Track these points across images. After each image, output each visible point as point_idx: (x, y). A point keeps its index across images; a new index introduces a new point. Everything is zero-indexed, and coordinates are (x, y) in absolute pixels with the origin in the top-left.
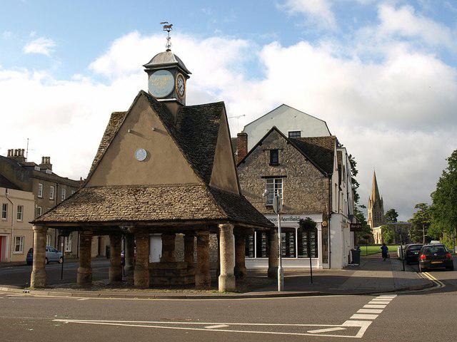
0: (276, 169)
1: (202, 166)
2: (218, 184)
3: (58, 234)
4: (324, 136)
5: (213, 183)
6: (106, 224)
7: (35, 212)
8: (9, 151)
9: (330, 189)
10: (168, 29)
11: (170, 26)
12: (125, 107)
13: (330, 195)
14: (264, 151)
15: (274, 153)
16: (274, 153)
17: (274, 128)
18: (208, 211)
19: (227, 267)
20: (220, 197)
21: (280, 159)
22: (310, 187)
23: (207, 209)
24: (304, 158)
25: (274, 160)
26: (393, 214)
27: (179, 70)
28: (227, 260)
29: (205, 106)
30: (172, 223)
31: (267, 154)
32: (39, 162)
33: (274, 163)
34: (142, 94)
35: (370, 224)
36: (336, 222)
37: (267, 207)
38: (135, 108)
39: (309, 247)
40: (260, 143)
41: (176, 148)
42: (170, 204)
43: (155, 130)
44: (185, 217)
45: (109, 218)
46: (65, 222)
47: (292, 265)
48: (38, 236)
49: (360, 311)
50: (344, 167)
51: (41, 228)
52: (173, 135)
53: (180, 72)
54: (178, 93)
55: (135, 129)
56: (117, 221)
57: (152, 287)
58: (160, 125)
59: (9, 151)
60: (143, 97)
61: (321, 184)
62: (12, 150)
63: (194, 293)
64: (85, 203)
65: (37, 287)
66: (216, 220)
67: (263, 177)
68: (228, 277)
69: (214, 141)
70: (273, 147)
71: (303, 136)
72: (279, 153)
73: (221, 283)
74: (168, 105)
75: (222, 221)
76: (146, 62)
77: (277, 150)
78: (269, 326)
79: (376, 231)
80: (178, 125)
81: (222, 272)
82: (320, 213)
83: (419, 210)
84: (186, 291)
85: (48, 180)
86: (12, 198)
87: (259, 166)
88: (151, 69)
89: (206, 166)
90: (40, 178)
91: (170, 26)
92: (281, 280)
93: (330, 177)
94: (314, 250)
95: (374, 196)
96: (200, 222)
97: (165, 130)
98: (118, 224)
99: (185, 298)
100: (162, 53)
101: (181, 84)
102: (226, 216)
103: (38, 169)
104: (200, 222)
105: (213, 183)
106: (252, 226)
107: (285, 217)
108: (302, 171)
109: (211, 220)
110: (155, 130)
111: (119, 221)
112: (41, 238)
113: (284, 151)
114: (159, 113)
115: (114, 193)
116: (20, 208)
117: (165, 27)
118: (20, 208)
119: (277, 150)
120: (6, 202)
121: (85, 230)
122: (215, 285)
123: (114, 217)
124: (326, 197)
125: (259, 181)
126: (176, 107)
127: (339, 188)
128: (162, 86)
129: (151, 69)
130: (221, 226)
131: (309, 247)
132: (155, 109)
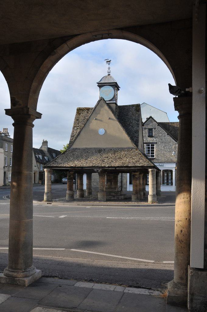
0: (152, 139)
1: (134, 137)
6: (86, 168)
7: (4, 160)
10: (109, 63)
11: (109, 61)
14: (145, 129)
15: (150, 130)
16: (150, 130)
21: (153, 134)
22: (169, 149)
25: (151, 134)
29: (130, 106)
30: (123, 168)
31: (147, 131)
33: (151, 136)
39: (168, 181)
42: (120, 158)
43: (109, 119)
45: (88, 165)
48: (48, 174)
51: (49, 170)
54: (115, 98)
56: (93, 167)
60: (102, 101)
66: (147, 167)
68: (153, 196)
70: (150, 127)
73: (150, 199)
75: (151, 167)
76: (98, 81)
77: (152, 129)
82: (175, 162)
90: (6, 141)
91: (109, 61)
94: (170, 181)
108: (165, 140)
109: (145, 167)
110: (109, 119)
111: (94, 167)
113: (156, 129)
115: (88, 152)
117: (107, 62)
119: (152, 129)
121: (71, 171)
122: (146, 200)
123: (91, 165)
126: (114, 105)
128: (108, 93)
130: (150, 170)
131: (168, 181)
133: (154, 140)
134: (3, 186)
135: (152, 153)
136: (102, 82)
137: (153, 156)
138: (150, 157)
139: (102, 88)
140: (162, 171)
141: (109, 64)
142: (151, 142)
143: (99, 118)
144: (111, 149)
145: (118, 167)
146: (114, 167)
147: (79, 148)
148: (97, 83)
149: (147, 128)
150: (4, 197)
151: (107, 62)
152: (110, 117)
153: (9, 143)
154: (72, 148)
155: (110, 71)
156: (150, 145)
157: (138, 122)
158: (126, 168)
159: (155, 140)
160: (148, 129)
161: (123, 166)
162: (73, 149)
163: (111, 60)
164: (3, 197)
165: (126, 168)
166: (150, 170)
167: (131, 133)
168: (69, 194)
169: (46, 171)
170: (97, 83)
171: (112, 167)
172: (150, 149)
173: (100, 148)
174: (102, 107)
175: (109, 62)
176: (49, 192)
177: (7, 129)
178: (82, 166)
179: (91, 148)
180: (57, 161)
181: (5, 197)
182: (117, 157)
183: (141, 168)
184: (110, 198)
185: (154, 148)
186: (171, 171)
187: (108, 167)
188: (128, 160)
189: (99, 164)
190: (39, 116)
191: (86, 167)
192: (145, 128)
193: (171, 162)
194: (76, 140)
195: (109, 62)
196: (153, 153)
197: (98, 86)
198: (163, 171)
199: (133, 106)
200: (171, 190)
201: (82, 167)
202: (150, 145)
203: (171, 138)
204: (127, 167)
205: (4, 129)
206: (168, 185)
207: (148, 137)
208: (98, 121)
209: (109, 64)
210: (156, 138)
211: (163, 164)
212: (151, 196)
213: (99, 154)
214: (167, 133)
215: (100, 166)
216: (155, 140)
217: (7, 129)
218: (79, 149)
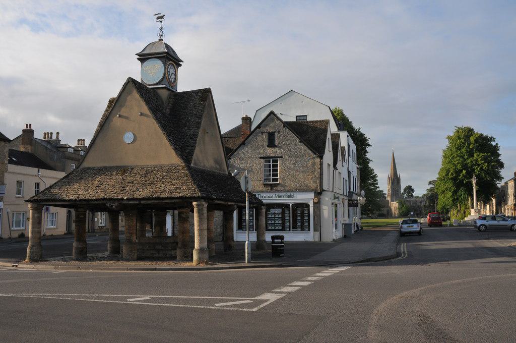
1: (184, 147)
4: (319, 119)
5: (195, 164)
6: (94, 202)
9: (321, 168)
10: (161, 20)
11: (162, 17)
13: (321, 174)
14: (262, 133)
15: (271, 136)
16: (271, 136)
17: (272, 113)
18: (188, 189)
19: (201, 242)
20: (200, 176)
22: (303, 166)
23: (184, 187)
24: (298, 141)
26: (410, 189)
27: (170, 59)
28: (200, 235)
29: (193, 92)
30: (152, 202)
31: (265, 136)
33: (271, 144)
35: (389, 199)
36: (327, 199)
37: (265, 185)
39: (303, 223)
41: (160, 131)
43: (142, 114)
44: (163, 195)
45: (97, 197)
47: (291, 237)
48: (33, 214)
49: (320, 278)
50: (343, 149)
52: (157, 119)
53: (172, 60)
54: (169, 81)
55: (121, 113)
56: (103, 199)
57: (140, 259)
58: (145, 109)
61: (314, 164)
62: (48, 133)
63: (172, 264)
64: (77, 182)
65: (33, 260)
67: (261, 158)
70: (270, 129)
71: (309, 119)
72: (276, 136)
74: (160, 91)
76: (139, 51)
78: (168, 298)
79: (394, 205)
80: (168, 110)
81: (197, 245)
83: (432, 186)
84: (165, 263)
86: (42, 177)
87: (258, 147)
88: (143, 58)
89: (189, 148)
90: (72, 159)
91: (162, 17)
92: (248, 253)
93: (321, 157)
95: (393, 172)
96: (177, 201)
97: (150, 114)
98: (105, 202)
99: (155, 269)
100: (154, 43)
101: (172, 71)
102: (199, 194)
103: (71, 150)
104: (177, 201)
107: (280, 194)
109: (186, 198)
110: (142, 114)
112: (36, 215)
113: (281, 133)
114: (148, 102)
117: (158, 18)
120: (37, 180)
122: (191, 259)
123: (102, 196)
124: (318, 176)
128: (153, 73)
129: (143, 58)
131: (303, 223)
132: (141, 95)
133: (277, 151)
134: (65, 234)
135: (274, 175)
136: (145, 52)
137: (277, 180)
138: (271, 182)
139: (146, 63)
140: (291, 205)
141: (161, 22)
142: (271, 155)
143: (124, 115)
145: (143, 199)
146: (137, 199)
147: (93, 168)
151: (158, 18)
152: (142, 112)
154: (82, 167)
156: (271, 161)
157: (199, 119)
158: (157, 202)
159: (278, 151)
161: (151, 197)
162: (84, 168)
163: (164, 15)
165: (157, 202)
166: (194, 203)
167: (184, 139)
168: (77, 248)
169: (31, 207)
171: (133, 199)
172: (271, 168)
174: (130, 93)
175: (161, 18)
176: (34, 244)
177: (84, 140)
178: (87, 198)
182: (148, 182)
183: (181, 200)
184: (152, 254)
185: (277, 166)
186: (308, 206)
187: (128, 199)
188: (163, 186)
189: (116, 195)
190: (449, 137)
191: (93, 200)
193: (306, 190)
194: (89, 154)
195: (161, 18)
196: (277, 175)
197: (138, 59)
198: (293, 205)
199: (198, 91)
200: (307, 240)
201: (88, 201)
202: (271, 161)
203: (306, 148)
204: (158, 198)
205: (79, 140)
206: (303, 229)
207: (268, 146)
208: (124, 120)
209: (161, 22)
210: (280, 148)
211: (292, 194)
212: (196, 251)
214: (299, 138)
215: (115, 197)
216: (278, 151)
217: (84, 140)
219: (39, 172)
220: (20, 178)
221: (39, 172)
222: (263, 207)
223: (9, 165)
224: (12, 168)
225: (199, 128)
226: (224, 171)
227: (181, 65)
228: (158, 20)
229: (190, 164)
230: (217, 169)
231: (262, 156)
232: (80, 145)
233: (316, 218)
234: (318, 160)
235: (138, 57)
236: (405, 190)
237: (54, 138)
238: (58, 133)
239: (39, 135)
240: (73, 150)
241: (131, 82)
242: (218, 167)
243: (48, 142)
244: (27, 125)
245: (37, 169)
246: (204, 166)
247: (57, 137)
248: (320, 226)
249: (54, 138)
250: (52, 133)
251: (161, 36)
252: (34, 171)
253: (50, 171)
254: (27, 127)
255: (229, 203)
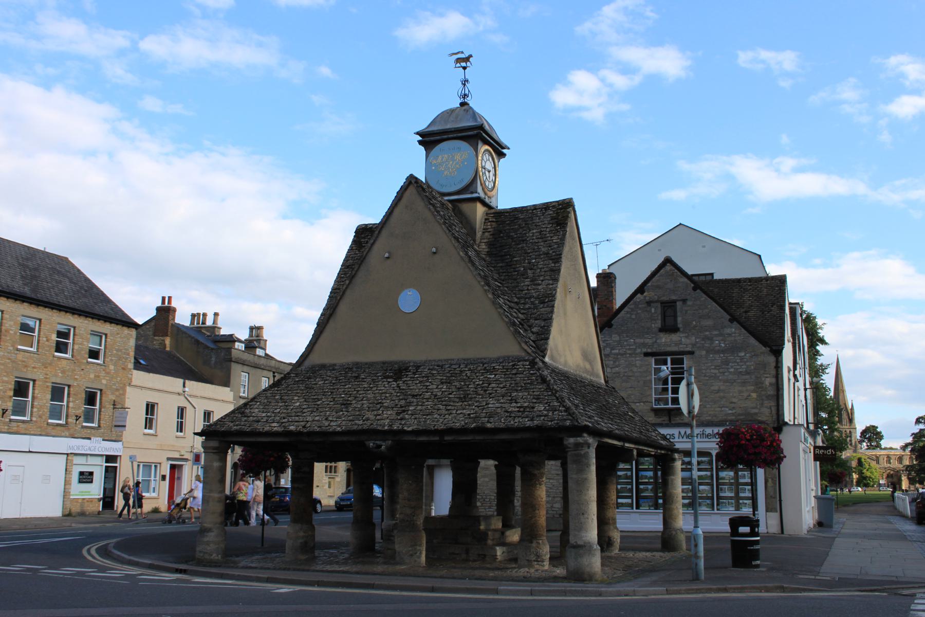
0: (675, 337)
2: (562, 360)
3: (718, 381)
5: (552, 358)
8: (193, 316)
10: (463, 64)
11: (467, 59)
12: (375, 218)
16: (668, 307)
17: (668, 261)
29: (535, 207)
30: (470, 438)
31: (656, 310)
32: (244, 335)
33: (669, 327)
34: (412, 181)
38: (397, 211)
40: (641, 290)
46: (261, 434)
53: (486, 142)
59: (193, 316)
60: (412, 190)
62: (199, 314)
69: (555, 273)
71: (716, 277)
76: (423, 126)
80: (483, 246)
85: (256, 367)
86: (190, 396)
90: (243, 363)
91: (467, 59)
105: (552, 358)
106: (632, 446)
113: (689, 303)
115: (357, 377)
116: (150, 408)
118: (150, 408)
119: (674, 302)
120: (183, 403)
125: (639, 361)
127: (795, 376)
141: (465, 68)
144: (442, 367)
145: (450, 431)
148: (418, 133)
149: (656, 302)
150: (89, 551)
151: (459, 60)
153: (253, 371)
155: (467, 92)
157: (555, 263)
160: (659, 305)
163: (471, 56)
164: (84, 552)
170: (418, 133)
173: (404, 363)
175: (464, 61)
179: (371, 365)
180: (247, 411)
181: (93, 552)
187: (413, 432)
192: (647, 298)
195: (464, 61)
197: (420, 142)
199: (546, 207)
201: (324, 434)
204: (481, 430)
209: (465, 68)
213: (394, 384)
215: (386, 428)
218: (332, 367)
219: (184, 386)
220: (153, 398)
221: (184, 386)
222: (676, 456)
223: (135, 372)
224: (140, 377)
225: (556, 280)
226: (598, 376)
227: (503, 155)
228: (458, 65)
229: (544, 357)
230: (586, 371)
231: (649, 350)
232: (254, 338)
233: (770, 483)
234: (771, 359)
235: (420, 138)
236: (864, 433)
237: (209, 322)
238: (216, 314)
239: (182, 318)
240: (243, 345)
241: (412, 181)
242: (588, 366)
243: (199, 330)
244: (164, 299)
245: (181, 381)
246: (566, 364)
247: (215, 322)
248: (780, 501)
249: (209, 322)
250: (205, 315)
251: (465, 96)
252: (175, 383)
253: (203, 384)
254: (163, 302)
255: (627, 445)
